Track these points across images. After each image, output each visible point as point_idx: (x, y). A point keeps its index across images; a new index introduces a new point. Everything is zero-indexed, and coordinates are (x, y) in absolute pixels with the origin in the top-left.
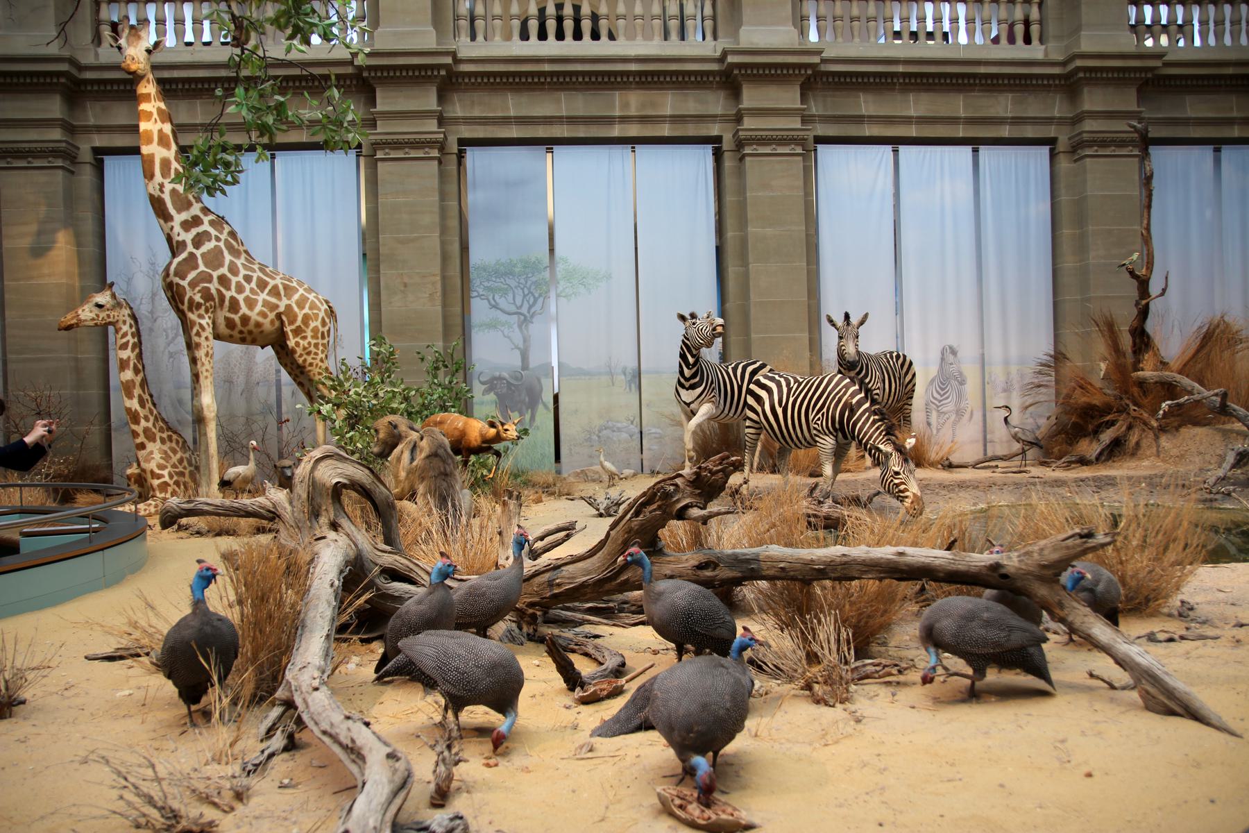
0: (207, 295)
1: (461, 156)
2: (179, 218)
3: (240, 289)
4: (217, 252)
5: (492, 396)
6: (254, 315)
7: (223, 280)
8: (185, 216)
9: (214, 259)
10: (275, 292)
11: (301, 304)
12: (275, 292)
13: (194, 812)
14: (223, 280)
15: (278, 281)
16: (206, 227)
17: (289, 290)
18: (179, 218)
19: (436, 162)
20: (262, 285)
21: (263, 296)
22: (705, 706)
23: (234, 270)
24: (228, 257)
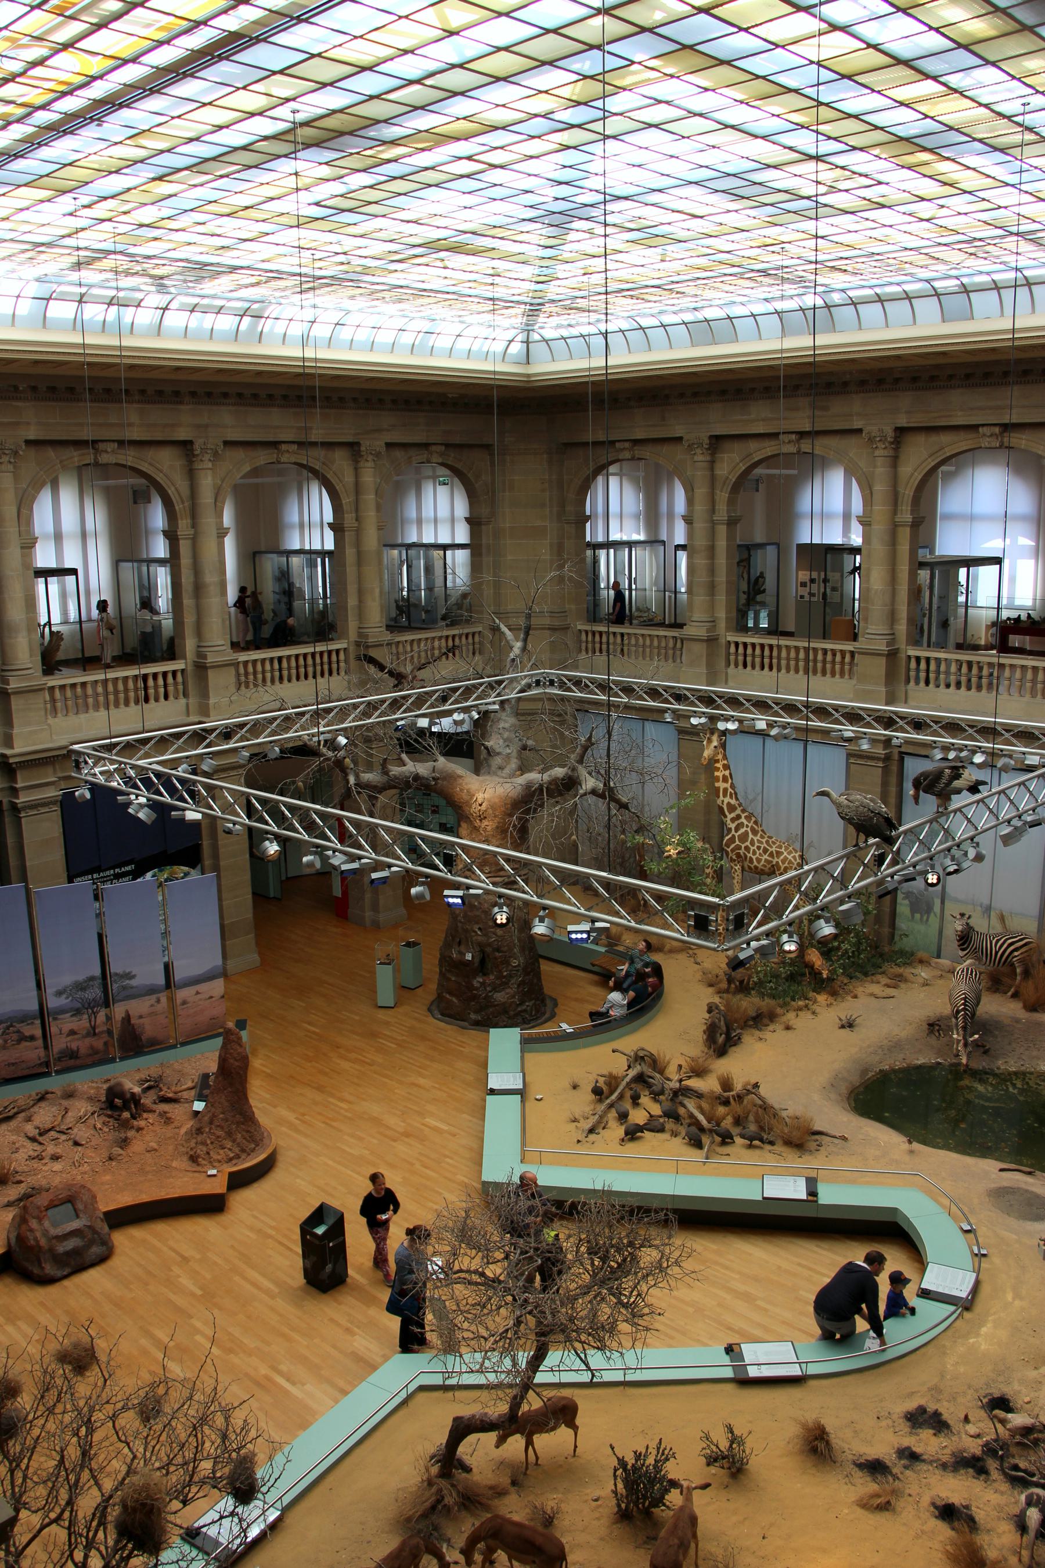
0: (738, 855)
1: (901, 760)
2: (730, 816)
3: (754, 853)
4: (746, 833)
5: (906, 902)
6: (760, 866)
7: (747, 848)
8: (733, 815)
9: (744, 838)
10: (771, 855)
11: (783, 862)
12: (771, 855)
13: (14, 1447)
14: (747, 848)
15: (774, 849)
16: (743, 820)
17: (779, 854)
18: (730, 816)
19: (883, 661)
20: (765, 851)
21: (766, 857)
22: (865, 1071)
23: (752, 843)
24: (751, 836)
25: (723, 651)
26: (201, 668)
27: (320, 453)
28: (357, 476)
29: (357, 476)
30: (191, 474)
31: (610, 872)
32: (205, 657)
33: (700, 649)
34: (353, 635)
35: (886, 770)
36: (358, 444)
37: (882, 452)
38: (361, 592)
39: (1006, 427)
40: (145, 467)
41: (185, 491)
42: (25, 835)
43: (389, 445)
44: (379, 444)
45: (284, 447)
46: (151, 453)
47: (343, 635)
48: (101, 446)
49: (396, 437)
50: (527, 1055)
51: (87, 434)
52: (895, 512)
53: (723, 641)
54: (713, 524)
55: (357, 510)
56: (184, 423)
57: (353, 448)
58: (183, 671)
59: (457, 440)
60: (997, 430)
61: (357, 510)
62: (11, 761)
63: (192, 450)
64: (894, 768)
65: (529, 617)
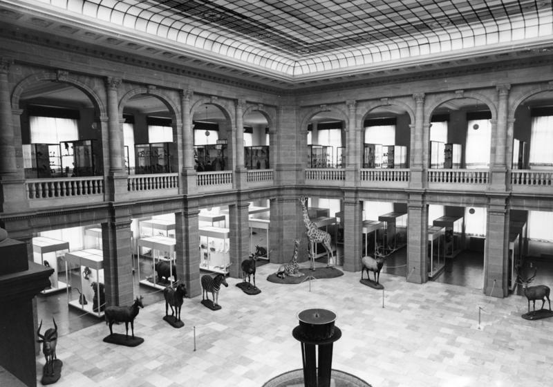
19: (421, 173)
25: (359, 175)
26: (185, 175)
27: (224, 101)
28: (236, 111)
29: (236, 111)
30: (181, 103)
31: (16, 280)
32: (186, 171)
33: (352, 174)
34: (234, 169)
35: (422, 210)
36: (237, 100)
37: (419, 101)
38: (237, 153)
39: (466, 90)
40: (165, 98)
41: (179, 109)
42: (117, 237)
43: (247, 102)
44: (244, 101)
45: (213, 97)
46: (167, 93)
47: (231, 169)
48: (150, 87)
49: (249, 99)
50: (44, 254)
51: (144, 81)
52: (423, 122)
53: (359, 171)
54: (356, 131)
55: (236, 124)
56: (180, 82)
57: (235, 101)
58: (177, 177)
59: (268, 103)
60: (462, 91)
61: (236, 124)
62: (114, 205)
63: (182, 93)
64: (425, 210)
65: (538, 18)
